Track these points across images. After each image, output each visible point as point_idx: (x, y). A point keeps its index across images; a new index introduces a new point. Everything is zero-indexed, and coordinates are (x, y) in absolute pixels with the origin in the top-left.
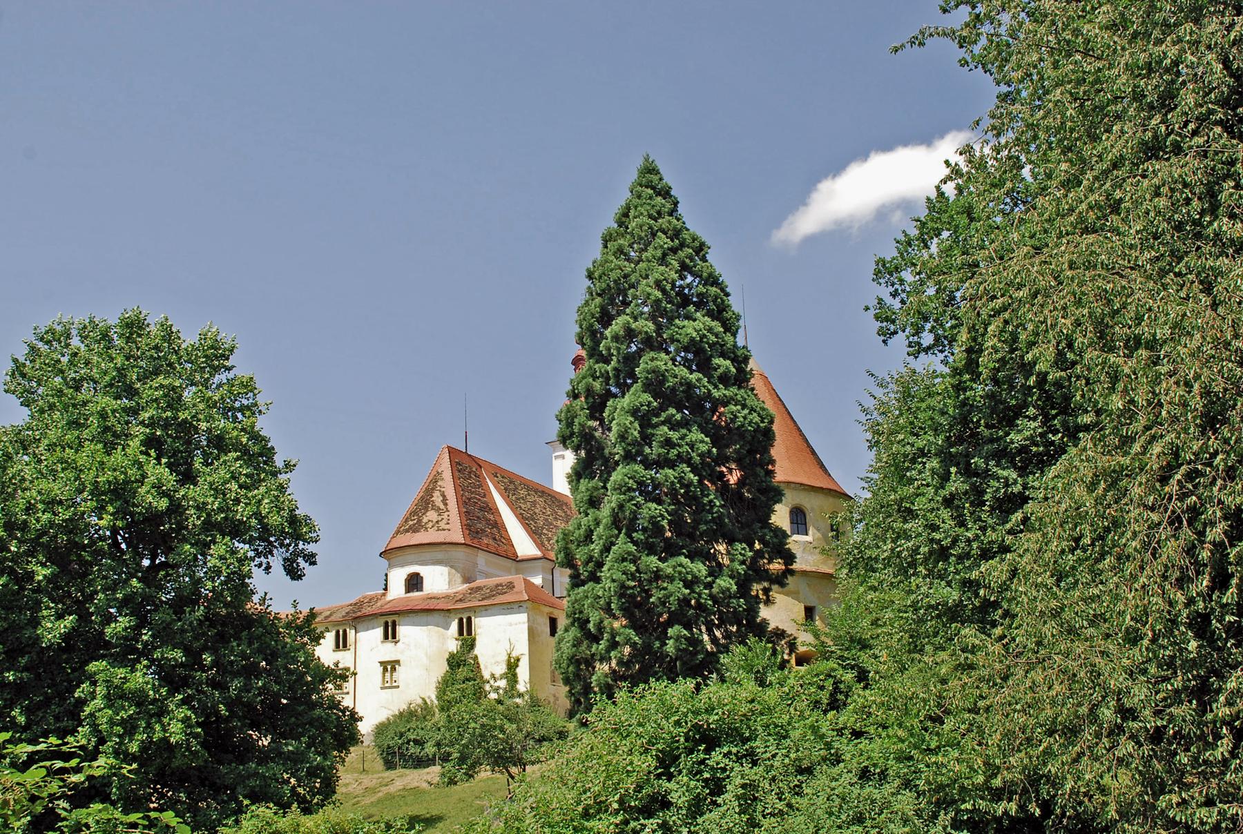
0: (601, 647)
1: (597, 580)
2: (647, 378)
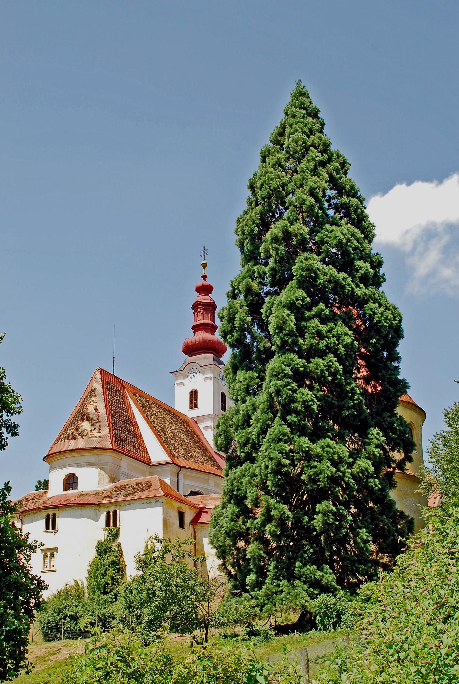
0: (256, 521)
1: (252, 460)
2: (302, 275)
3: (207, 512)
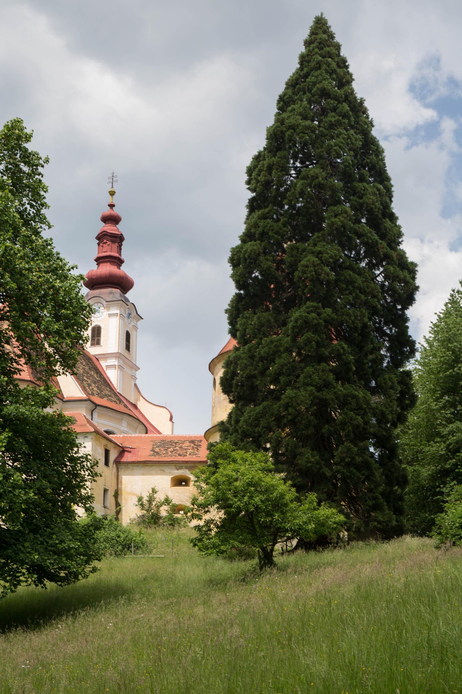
3: (130, 452)
